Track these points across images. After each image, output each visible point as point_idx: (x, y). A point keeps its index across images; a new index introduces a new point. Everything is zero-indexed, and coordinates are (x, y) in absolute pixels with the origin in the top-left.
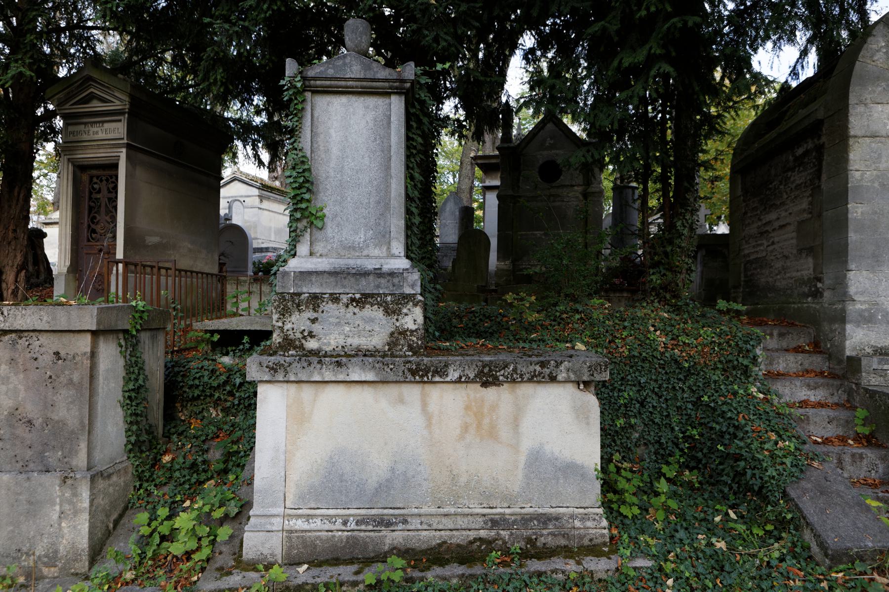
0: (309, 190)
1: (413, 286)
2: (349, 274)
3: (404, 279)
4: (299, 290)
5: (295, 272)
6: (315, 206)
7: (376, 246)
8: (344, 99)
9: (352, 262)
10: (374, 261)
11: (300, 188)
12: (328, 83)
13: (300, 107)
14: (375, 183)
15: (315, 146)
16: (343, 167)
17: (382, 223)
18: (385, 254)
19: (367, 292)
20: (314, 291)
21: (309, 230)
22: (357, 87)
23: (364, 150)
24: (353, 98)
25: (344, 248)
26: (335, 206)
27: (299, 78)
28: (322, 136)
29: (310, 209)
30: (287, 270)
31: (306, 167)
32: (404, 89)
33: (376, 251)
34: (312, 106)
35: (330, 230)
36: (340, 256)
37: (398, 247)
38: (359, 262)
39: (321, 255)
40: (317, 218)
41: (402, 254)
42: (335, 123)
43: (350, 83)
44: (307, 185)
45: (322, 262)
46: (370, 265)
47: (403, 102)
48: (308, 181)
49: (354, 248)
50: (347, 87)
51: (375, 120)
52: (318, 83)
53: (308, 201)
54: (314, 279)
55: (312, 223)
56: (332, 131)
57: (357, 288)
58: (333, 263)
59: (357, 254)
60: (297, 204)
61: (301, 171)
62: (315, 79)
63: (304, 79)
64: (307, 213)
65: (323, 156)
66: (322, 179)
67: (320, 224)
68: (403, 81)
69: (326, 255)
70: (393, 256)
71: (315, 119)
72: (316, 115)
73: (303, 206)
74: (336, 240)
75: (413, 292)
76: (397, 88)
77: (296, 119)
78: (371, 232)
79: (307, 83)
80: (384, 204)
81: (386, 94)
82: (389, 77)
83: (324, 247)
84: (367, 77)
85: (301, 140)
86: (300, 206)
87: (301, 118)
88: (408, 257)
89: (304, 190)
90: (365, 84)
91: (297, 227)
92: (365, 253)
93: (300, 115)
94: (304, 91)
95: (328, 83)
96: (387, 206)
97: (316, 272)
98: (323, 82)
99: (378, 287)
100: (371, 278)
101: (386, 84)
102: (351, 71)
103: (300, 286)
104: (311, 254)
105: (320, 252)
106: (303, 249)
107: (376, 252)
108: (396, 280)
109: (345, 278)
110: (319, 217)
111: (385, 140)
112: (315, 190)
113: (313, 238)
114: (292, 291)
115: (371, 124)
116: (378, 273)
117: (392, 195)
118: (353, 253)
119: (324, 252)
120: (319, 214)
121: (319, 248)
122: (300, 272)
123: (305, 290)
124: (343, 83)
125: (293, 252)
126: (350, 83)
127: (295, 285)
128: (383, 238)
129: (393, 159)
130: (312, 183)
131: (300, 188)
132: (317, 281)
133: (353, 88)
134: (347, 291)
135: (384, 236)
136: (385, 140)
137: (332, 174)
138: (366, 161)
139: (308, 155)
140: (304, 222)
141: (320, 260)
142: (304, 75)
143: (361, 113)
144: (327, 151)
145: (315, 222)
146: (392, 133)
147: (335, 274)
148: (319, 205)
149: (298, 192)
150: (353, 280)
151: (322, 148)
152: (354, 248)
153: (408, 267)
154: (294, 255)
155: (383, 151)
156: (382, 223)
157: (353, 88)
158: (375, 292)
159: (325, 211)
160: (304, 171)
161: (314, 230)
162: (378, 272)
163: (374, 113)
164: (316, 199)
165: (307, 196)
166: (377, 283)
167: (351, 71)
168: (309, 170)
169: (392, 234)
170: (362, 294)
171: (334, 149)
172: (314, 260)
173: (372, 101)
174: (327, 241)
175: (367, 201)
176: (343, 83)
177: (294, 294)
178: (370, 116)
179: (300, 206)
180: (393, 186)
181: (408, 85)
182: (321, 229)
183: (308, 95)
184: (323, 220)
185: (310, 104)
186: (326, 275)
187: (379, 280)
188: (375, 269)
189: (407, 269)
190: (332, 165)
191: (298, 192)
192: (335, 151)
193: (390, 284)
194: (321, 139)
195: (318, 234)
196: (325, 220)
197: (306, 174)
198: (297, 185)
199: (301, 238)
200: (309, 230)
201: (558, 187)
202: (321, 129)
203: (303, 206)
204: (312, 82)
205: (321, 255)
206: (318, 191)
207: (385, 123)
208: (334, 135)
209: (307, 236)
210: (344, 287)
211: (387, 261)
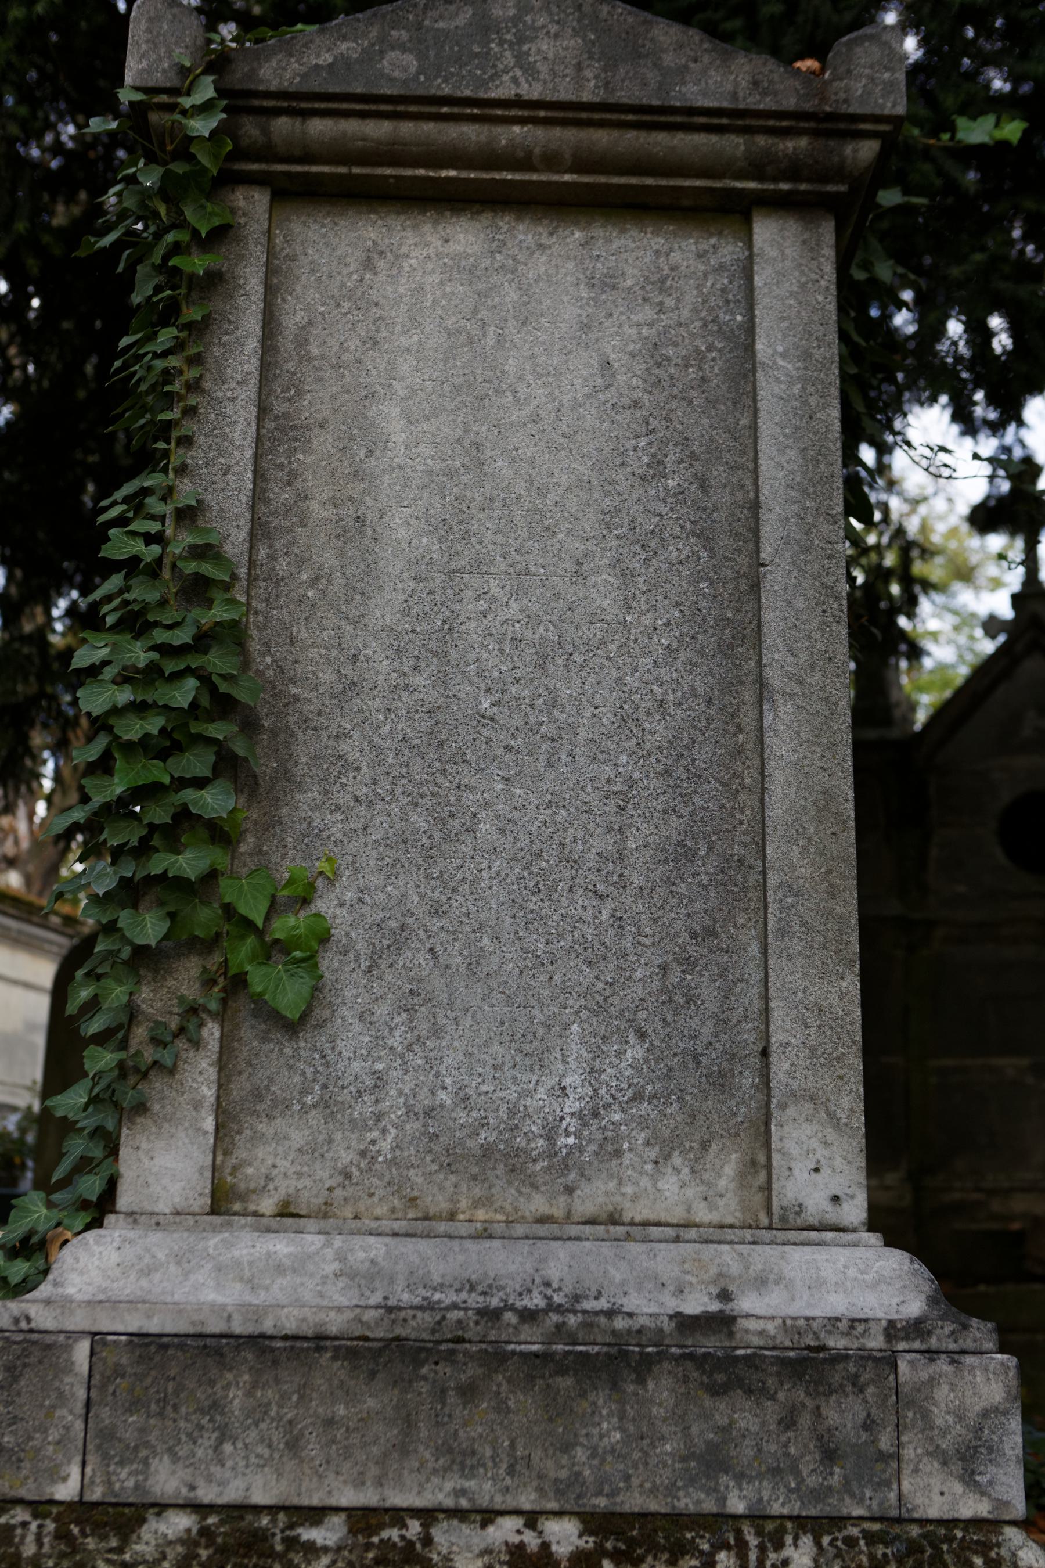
0: (229, 766)
1: (968, 1461)
2: (496, 1358)
3: (906, 1406)
4: (125, 1480)
5: (96, 1337)
6: (263, 869)
7: (666, 1148)
8: (464, 237)
9: (506, 1267)
10: (666, 1259)
11: (166, 746)
12: (378, 130)
13: (197, 263)
14: (659, 729)
15: (280, 496)
16: (449, 628)
17: (708, 992)
18: (728, 1208)
19: (634, 1501)
20: (232, 1494)
21: (212, 1032)
22: (551, 161)
23: (588, 526)
24: (523, 234)
25: (451, 1161)
26: (391, 870)
27: (206, 91)
28: (324, 442)
29: (227, 891)
30: (43, 1318)
31: (219, 613)
32: (839, 173)
33: (669, 1185)
34: (271, 271)
35: (357, 1035)
36: (423, 1222)
37: (824, 1162)
38: (562, 1264)
39: (286, 1212)
40: (272, 950)
41: (855, 1211)
42: (405, 366)
43: (514, 134)
44: (217, 730)
45: (299, 1265)
46: (649, 1288)
47: (829, 252)
48: (224, 705)
49: (516, 1164)
50: (492, 159)
51: (654, 352)
52: (319, 128)
53: (220, 834)
54: (236, 1399)
55: (239, 982)
56: (390, 418)
57: (556, 1470)
58: (373, 1274)
59: (538, 1204)
60: (143, 850)
61: (182, 637)
62: (300, 103)
63: (238, 101)
64: (204, 917)
65: (328, 559)
66: (313, 702)
67: (289, 997)
68: (837, 125)
69: (324, 1212)
70: (775, 1221)
71: (286, 343)
72: (292, 319)
73: (188, 863)
74: (393, 1100)
75: (972, 1507)
76: (793, 171)
77: (166, 336)
78: (635, 1051)
79: (250, 129)
80: (721, 869)
81: (724, 209)
82: (753, 101)
83: (312, 1151)
84: (623, 95)
85: (194, 457)
86: (159, 863)
87: (199, 329)
88: (889, 1223)
89: (196, 763)
90: (602, 138)
91: (132, 1013)
92: (593, 1196)
93: (192, 313)
94: (231, 178)
95: (378, 130)
96: (743, 881)
97: (257, 1342)
98: (351, 126)
99: (713, 1462)
100: (661, 1391)
101: (734, 145)
102: (521, 59)
103: (137, 1454)
104: (223, 1201)
105: (283, 1188)
106: (164, 1162)
107: (669, 1192)
108: (843, 1415)
109: (468, 1392)
110: (283, 947)
111: (718, 473)
112: (265, 766)
113: (241, 1086)
114: (66, 1491)
115: (629, 379)
116: (709, 1353)
117: (776, 811)
118: (507, 1196)
119: (310, 1185)
120: (288, 925)
121: (279, 1157)
122: (141, 1339)
123: (166, 1480)
124: (470, 134)
125: (91, 1186)
126: (514, 134)
127: (100, 1443)
128: (722, 1094)
129: (777, 579)
130: (250, 726)
131: (166, 746)
132: (258, 1413)
133: (525, 164)
134: (485, 1490)
135: (720, 1081)
136: (718, 473)
137: (380, 666)
138: (603, 593)
139: (235, 541)
140: (186, 979)
141: (281, 1246)
142: (237, 78)
143: (570, 312)
144: (355, 528)
145: (258, 979)
146: (767, 428)
147: (404, 1359)
148: (288, 865)
149: (159, 772)
150: (524, 1405)
151: (318, 510)
152: (516, 1164)
153: (915, 1307)
154: (100, 1209)
155: (705, 537)
156: (708, 992)
157: (525, 164)
158: (686, 1503)
159: (325, 905)
160: (203, 640)
161: (248, 1032)
162: (710, 1344)
163: (648, 313)
164: (270, 825)
165: (214, 802)
166: (701, 1433)
167: (521, 59)
168: (232, 635)
169: (780, 1067)
170: (594, 1523)
171: (398, 517)
172: (247, 1245)
173: (634, 251)
174: (327, 1106)
175: (605, 844)
176: (470, 134)
177: (81, 1510)
178: (623, 333)
179: (159, 863)
180: (781, 748)
181: (867, 150)
182: (293, 1027)
183: (252, 205)
184: (310, 962)
185: (257, 254)
186: (330, 1370)
187: (721, 1411)
188: (686, 1323)
189: (917, 1328)
190: (382, 612)
191: (159, 772)
192: (403, 531)
193: (800, 1445)
194: (316, 460)
195: (277, 1065)
196: (329, 961)
197: (216, 661)
198: (154, 725)
199: (157, 1083)
200: (212, 1032)
201: (28, 1301)
202: (318, 400)
203: (188, 863)
204: (282, 125)
205: (286, 1212)
206: (285, 774)
207: (715, 370)
208: (397, 432)
209: (200, 1076)
210: (461, 1459)
211: (763, 1256)
